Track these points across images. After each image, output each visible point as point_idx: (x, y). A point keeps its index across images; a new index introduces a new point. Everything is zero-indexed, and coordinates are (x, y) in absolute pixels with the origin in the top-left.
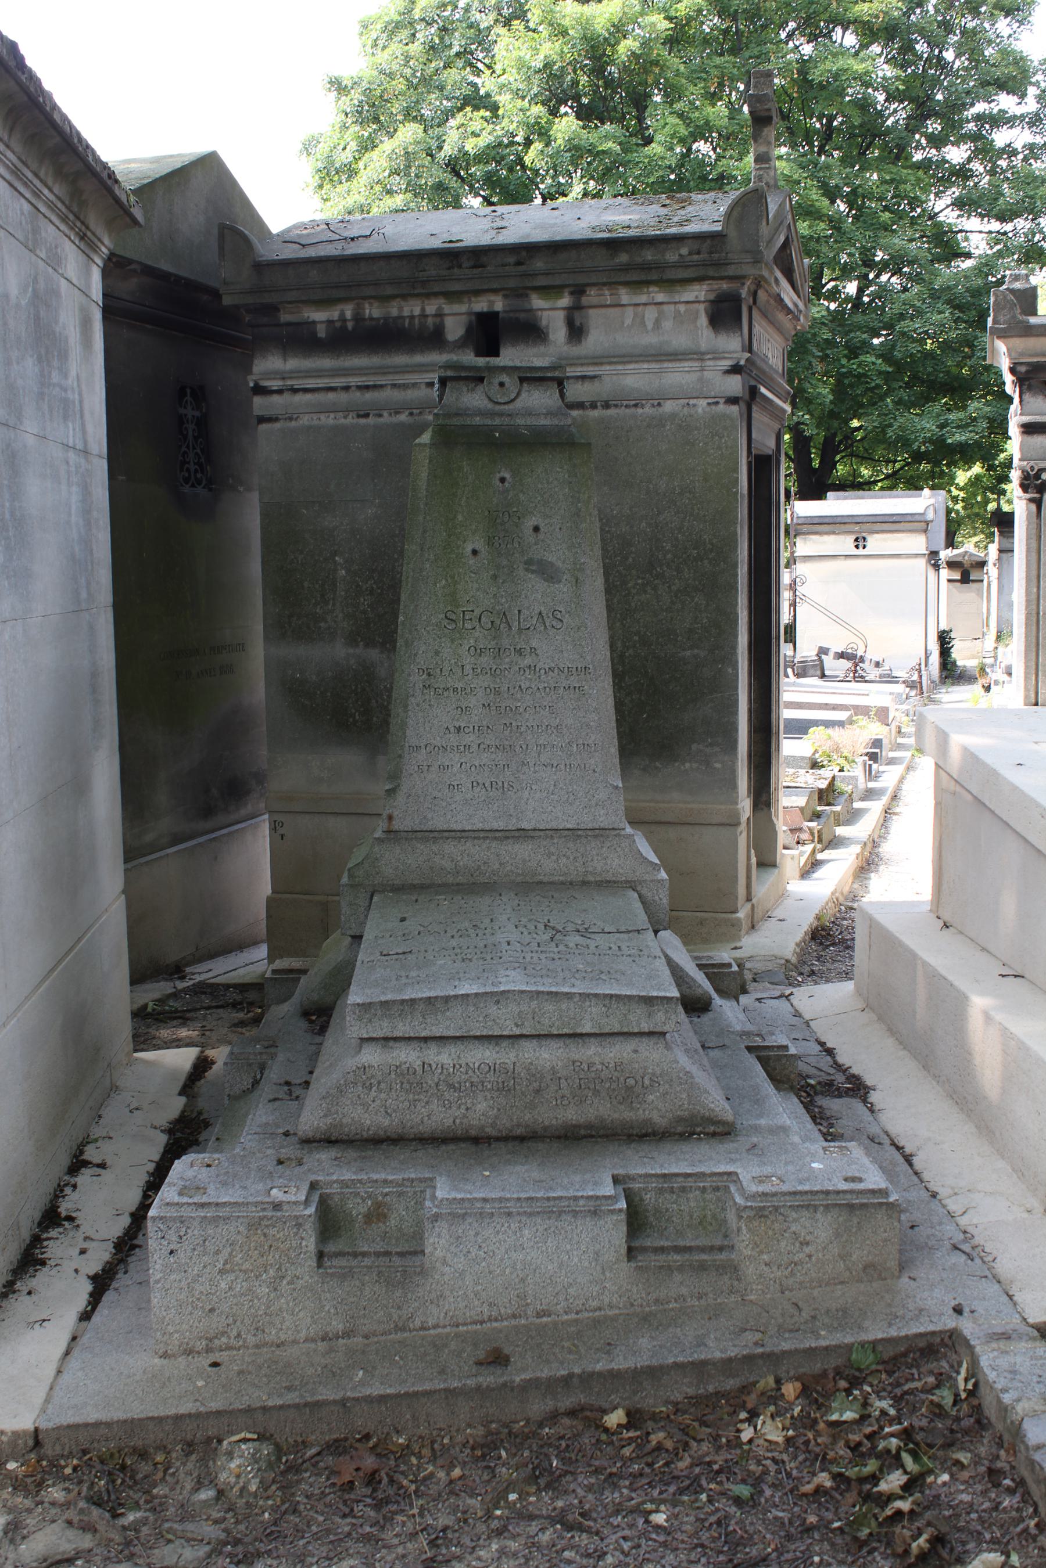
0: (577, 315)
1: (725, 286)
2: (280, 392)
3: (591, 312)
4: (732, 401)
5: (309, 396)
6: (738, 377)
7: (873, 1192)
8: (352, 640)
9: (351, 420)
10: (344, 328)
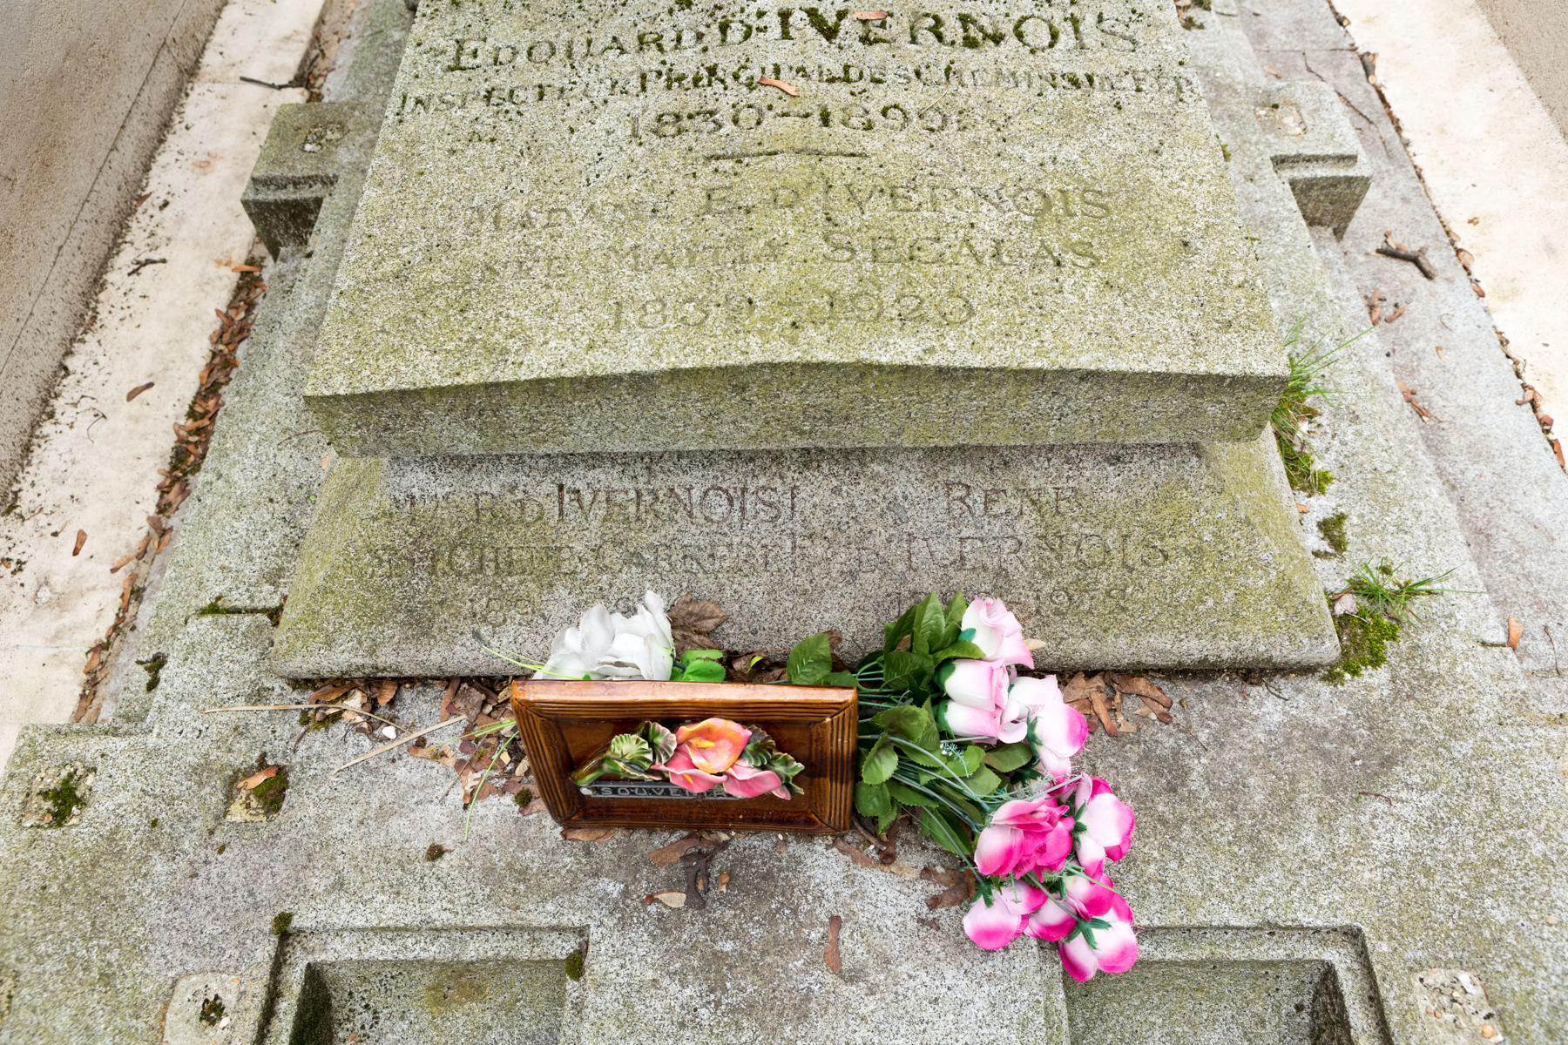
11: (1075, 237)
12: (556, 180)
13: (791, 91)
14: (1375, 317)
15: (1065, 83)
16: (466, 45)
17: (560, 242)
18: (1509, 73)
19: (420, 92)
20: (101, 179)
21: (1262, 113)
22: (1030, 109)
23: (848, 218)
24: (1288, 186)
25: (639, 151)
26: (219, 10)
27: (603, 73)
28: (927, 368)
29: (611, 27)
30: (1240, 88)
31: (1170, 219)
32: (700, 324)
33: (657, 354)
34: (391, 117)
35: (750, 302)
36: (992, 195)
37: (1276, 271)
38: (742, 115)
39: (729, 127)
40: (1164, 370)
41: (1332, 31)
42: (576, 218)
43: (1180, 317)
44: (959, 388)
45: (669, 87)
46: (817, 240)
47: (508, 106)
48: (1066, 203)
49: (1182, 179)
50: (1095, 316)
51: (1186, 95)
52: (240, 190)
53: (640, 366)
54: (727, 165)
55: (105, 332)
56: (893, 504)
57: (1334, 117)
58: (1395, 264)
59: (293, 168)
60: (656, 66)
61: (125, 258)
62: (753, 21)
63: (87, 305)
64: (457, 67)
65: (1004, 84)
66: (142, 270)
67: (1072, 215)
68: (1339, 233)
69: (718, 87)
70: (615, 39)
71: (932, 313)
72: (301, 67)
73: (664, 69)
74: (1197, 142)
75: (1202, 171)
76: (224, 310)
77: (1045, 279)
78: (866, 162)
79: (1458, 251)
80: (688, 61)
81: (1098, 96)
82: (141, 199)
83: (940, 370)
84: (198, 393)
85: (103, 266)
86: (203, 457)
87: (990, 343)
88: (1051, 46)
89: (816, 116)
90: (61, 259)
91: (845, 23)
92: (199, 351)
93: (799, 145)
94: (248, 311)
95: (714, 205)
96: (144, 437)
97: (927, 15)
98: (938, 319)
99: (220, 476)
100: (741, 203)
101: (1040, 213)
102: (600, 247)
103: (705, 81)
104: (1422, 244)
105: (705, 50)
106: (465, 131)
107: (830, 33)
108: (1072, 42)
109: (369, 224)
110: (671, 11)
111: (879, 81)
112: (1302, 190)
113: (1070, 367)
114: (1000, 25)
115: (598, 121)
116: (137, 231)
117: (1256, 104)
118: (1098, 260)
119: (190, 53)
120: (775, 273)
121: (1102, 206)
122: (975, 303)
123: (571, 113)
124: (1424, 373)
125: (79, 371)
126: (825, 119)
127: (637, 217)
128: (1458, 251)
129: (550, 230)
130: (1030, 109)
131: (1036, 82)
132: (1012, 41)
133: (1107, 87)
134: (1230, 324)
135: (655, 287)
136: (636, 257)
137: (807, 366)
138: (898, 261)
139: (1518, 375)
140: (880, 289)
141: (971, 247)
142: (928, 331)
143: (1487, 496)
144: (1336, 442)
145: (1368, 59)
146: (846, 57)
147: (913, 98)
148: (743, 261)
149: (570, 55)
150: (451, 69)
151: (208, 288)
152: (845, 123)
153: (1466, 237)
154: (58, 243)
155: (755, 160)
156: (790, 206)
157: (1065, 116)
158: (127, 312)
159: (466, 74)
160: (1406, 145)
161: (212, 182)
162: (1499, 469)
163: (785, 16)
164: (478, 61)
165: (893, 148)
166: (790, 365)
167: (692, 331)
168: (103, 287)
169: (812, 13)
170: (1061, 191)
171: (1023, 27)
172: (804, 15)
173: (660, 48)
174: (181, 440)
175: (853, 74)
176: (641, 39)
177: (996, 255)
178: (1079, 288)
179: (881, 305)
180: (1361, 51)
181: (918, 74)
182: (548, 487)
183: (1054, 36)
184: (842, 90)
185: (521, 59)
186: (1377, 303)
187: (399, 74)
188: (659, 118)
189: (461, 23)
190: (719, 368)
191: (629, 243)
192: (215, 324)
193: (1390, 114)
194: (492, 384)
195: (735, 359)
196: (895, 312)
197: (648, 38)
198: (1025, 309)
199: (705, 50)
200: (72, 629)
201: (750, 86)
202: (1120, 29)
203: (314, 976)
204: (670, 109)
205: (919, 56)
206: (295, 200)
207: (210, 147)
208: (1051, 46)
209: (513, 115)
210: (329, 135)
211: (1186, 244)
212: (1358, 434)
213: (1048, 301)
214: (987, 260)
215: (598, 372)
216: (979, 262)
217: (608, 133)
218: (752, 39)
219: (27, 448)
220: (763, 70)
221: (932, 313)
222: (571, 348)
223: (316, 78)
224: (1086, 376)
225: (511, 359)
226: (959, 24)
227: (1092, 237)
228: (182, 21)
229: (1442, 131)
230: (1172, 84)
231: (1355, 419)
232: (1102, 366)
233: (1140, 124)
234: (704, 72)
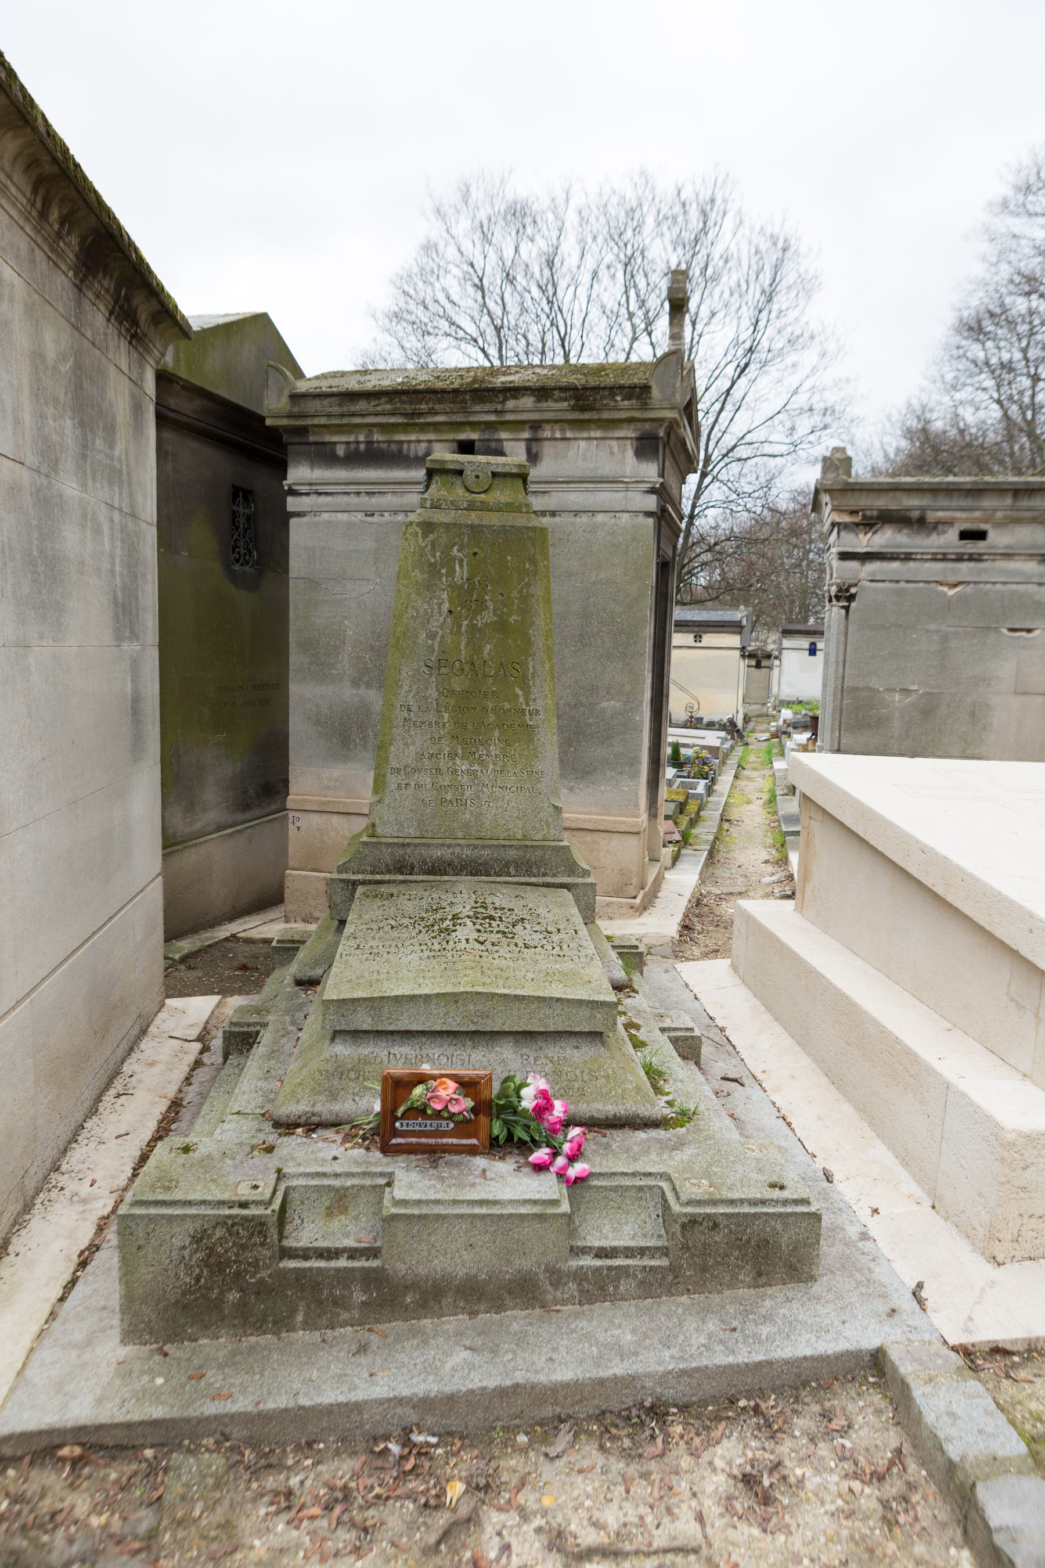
0: (534, 444)
1: (647, 426)
2: (307, 494)
3: (546, 444)
4: (649, 514)
5: (329, 499)
6: (654, 497)
7: (797, 1202)
8: (356, 683)
9: (360, 516)
10: (357, 449)
18: (778, 1029)
56: (503, 1061)
61: (112, 1092)
112: (675, 1041)
182: (385, 1052)
200: (91, 1210)
203: (287, 1189)
219: (65, 1151)
224: (558, 1000)
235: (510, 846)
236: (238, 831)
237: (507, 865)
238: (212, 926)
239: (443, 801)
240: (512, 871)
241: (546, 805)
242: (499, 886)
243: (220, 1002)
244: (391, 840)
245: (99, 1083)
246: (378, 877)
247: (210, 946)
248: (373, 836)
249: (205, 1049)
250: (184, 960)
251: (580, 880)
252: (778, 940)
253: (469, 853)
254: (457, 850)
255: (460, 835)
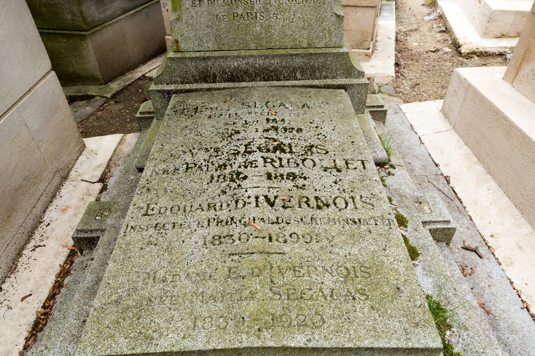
11: (359, 286)
12: (176, 262)
13: (259, 228)
14: (465, 274)
15: (351, 222)
16: (150, 206)
17: (176, 290)
18: (493, 184)
19: (133, 224)
20: (28, 218)
21: (417, 205)
22: (340, 234)
23: (279, 281)
24: (428, 231)
25: (206, 251)
26: (78, 157)
27: (196, 218)
28: (308, 348)
29: (199, 201)
30: (408, 196)
31: (392, 278)
32: (225, 328)
33: (208, 342)
34: (122, 233)
35: (243, 318)
36: (329, 269)
37: (429, 266)
38: (242, 237)
39: (237, 242)
40: (396, 346)
41: (434, 169)
42: (182, 279)
43: (400, 321)
44: (321, 353)
45: (217, 225)
46: (267, 291)
47: (162, 231)
48: (355, 272)
49: (394, 261)
50: (369, 322)
51: (392, 226)
52: (72, 233)
53: (202, 348)
54: (236, 258)
55: (19, 273)
57: (440, 207)
58: (468, 253)
59: (91, 226)
60: (213, 216)
61: (31, 245)
62: (246, 200)
63: (14, 263)
64: (146, 214)
65: (331, 223)
66: (37, 249)
67: (357, 277)
68: (448, 244)
69: (234, 225)
70: (200, 205)
71: (309, 323)
72: (102, 176)
73: (216, 218)
74: (398, 245)
75: (401, 257)
76: (62, 264)
77: (349, 306)
78: (284, 256)
79: (489, 247)
80: (224, 215)
81: (363, 228)
82: (41, 222)
83: (313, 349)
84: (48, 298)
85: (23, 248)
86: (45, 325)
87: (331, 336)
88: (346, 208)
89: (267, 238)
90: (8, 248)
91: (277, 200)
92: (51, 280)
93: (261, 250)
94: (71, 265)
95: (231, 275)
96: (24, 316)
97: (304, 197)
98: (312, 325)
99: (46, 348)
100: (241, 274)
101: (346, 277)
102: (190, 292)
103: (230, 223)
104: (476, 245)
105: (230, 210)
106: (146, 241)
107: (272, 205)
108: (353, 206)
109: (109, 279)
110: (219, 195)
111: (289, 223)
112: (433, 232)
113: (361, 346)
114: (329, 200)
115: (193, 238)
116: (37, 236)
117: (414, 202)
118: (368, 296)
119: (66, 172)
120: (252, 306)
121: (368, 273)
122: (325, 317)
123: (183, 234)
124: (486, 296)
125: (6, 289)
126: (270, 239)
127: (204, 279)
128: (489, 247)
129: (173, 283)
130: (340, 234)
131: (342, 222)
132: (333, 206)
133: (365, 224)
134: (417, 324)
135: (209, 311)
136: (203, 297)
137: (264, 348)
138: (297, 299)
139: (520, 297)
140: (290, 312)
141: (322, 292)
142: (308, 331)
143: (519, 349)
144: (460, 339)
145: (447, 178)
146: (278, 214)
147: (300, 230)
148: (241, 300)
149: (185, 211)
150: (144, 215)
151: (58, 256)
152: (277, 240)
153: (491, 242)
154: (8, 243)
155: (246, 256)
156: (258, 276)
157: (352, 236)
158: (28, 265)
159: (149, 217)
160: (465, 208)
161: (66, 216)
162: (521, 337)
163: (257, 198)
164: (154, 212)
165: (294, 250)
166: (258, 348)
167: (222, 331)
168: (21, 256)
169: (266, 197)
170: (353, 267)
171: (336, 201)
172: (263, 198)
173: (215, 209)
174: (38, 318)
175: (280, 221)
176: (209, 205)
177: (332, 296)
178: (362, 308)
179: (291, 319)
180: (445, 175)
181: (302, 220)
183: (347, 204)
184: (276, 227)
185: (168, 212)
186: (465, 268)
187: (127, 216)
188: (213, 238)
189: (150, 197)
190: (231, 349)
191: (201, 290)
192: (57, 269)
193: (457, 197)
194: (146, 353)
195: (237, 345)
196: (296, 323)
197: (211, 205)
198: (343, 320)
199: (230, 210)
201: (245, 225)
202: (368, 201)
204: (217, 234)
205: (302, 213)
206: (91, 237)
207: (67, 204)
208: (346, 208)
209: (163, 234)
210: (105, 214)
211: (398, 289)
212: (468, 335)
213: (351, 315)
214: (328, 298)
215: (186, 350)
216: (326, 299)
217: (196, 243)
218: (246, 207)
220: (249, 219)
221: (309, 323)
222: (177, 338)
223: (106, 179)
224: (367, 349)
225: (154, 343)
226: (315, 200)
227: (365, 286)
228: (65, 162)
229: (476, 203)
230: (387, 222)
231: (466, 329)
232: (373, 346)
233: (378, 238)
234: (229, 219)
235: (297, 55)
236: (138, 11)
237: (294, 71)
238: (133, 69)
239: (235, 16)
240: (298, 75)
241: (330, 14)
242: (288, 93)
243: (122, 139)
244: (193, 55)
245: (20, 239)
246: (188, 87)
247: (129, 85)
248: (177, 51)
249: (104, 189)
250: (113, 97)
251: (355, 81)
252: (505, 118)
253: (261, 62)
254: (251, 60)
255: (252, 46)
